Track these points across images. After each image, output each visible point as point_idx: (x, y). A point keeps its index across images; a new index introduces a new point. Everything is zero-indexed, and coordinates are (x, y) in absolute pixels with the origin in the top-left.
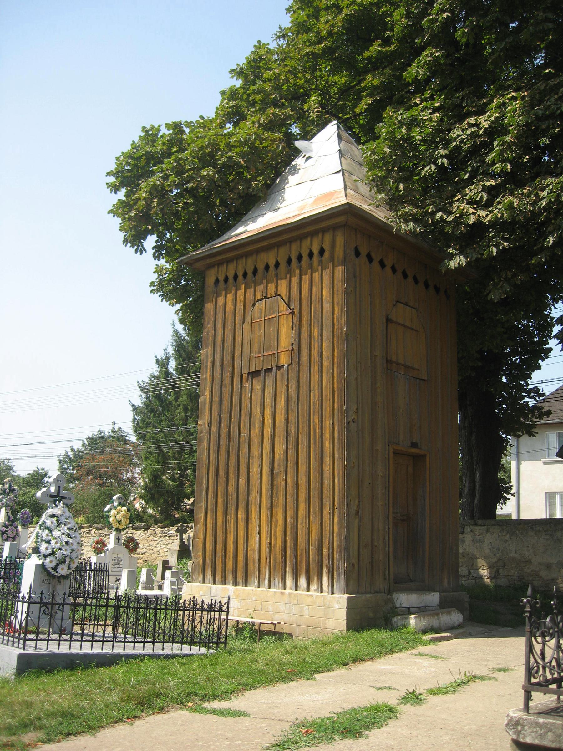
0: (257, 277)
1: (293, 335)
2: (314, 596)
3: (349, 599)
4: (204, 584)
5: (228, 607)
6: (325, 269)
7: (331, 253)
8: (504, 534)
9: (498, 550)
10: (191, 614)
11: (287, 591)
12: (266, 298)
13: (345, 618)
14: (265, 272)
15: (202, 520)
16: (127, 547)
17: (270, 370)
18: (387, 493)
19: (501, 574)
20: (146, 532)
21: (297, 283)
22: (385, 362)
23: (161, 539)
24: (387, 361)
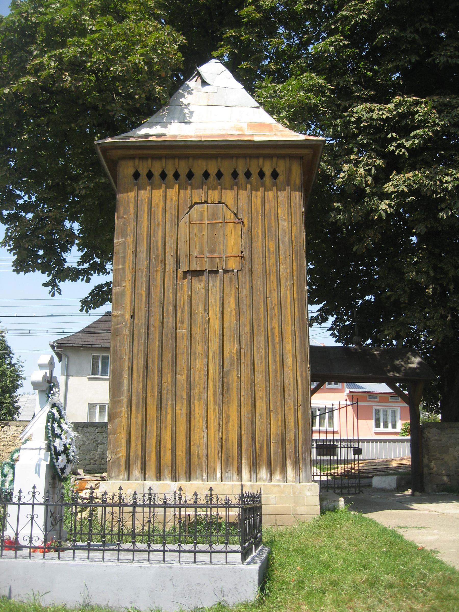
2: (282, 486)
6: (268, 191)
12: (206, 202)
17: (216, 272)
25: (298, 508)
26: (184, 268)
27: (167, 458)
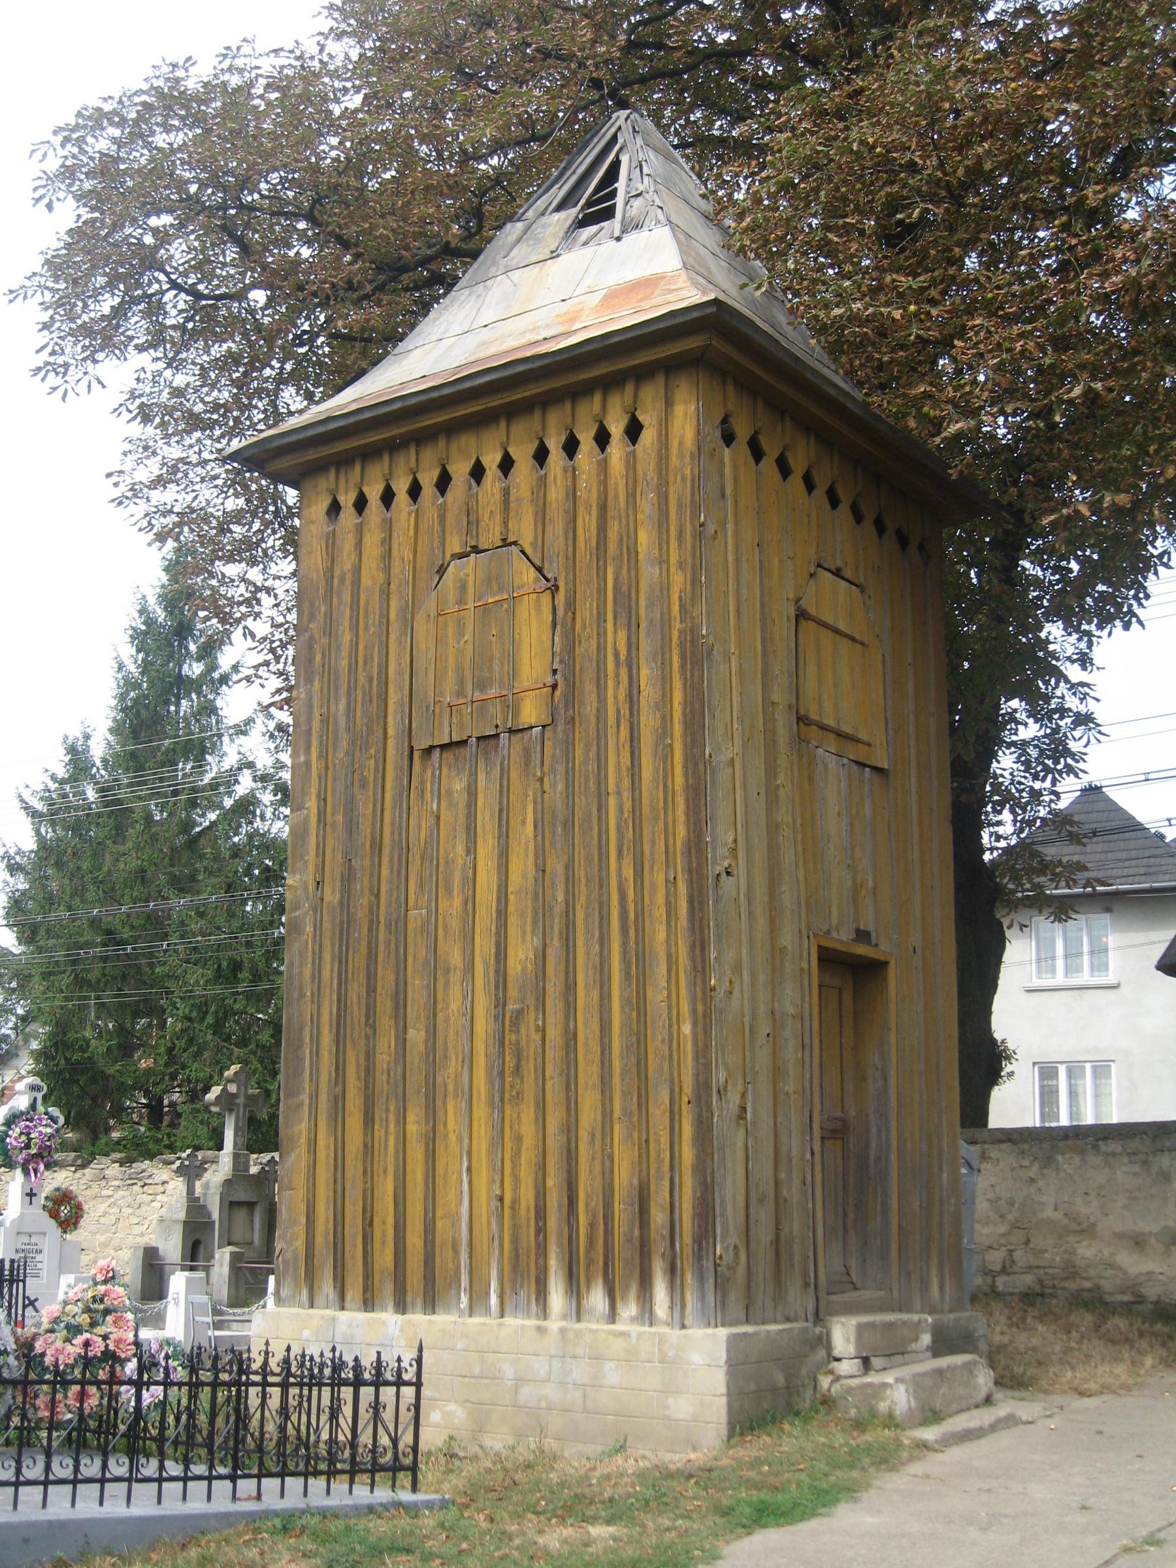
0: (450, 494)
1: (557, 649)
2: (634, 1336)
3: (733, 1341)
4: (311, 1311)
5: (419, 1373)
7: (660, 435)
8: (1026, 1163)
9: (1011, 1203)
10: (306, 1392)
11: (554, 1324)
13: (724, 1390)
14: (474, 484)
15: (303, 1140)
16: (54, 1214)
18: (807, 1059)
19: (1020, 1264)
20: (78, 1175)
21: (566, 512)
22: (794, 719)
23: (121, 1193)
24: (798, 719)
25: (671, 1401)
26: (422, 743)
27: (385, 1257)
